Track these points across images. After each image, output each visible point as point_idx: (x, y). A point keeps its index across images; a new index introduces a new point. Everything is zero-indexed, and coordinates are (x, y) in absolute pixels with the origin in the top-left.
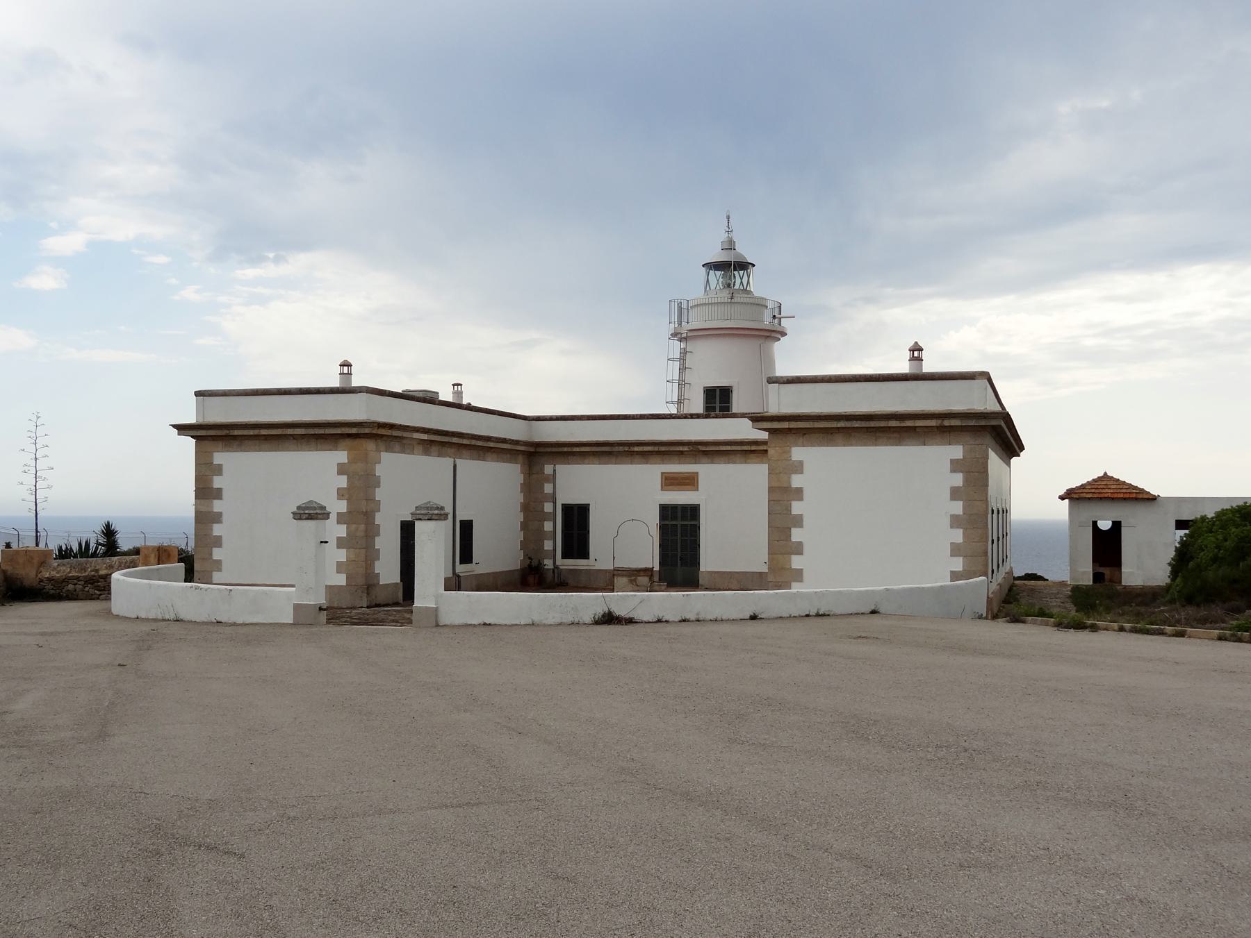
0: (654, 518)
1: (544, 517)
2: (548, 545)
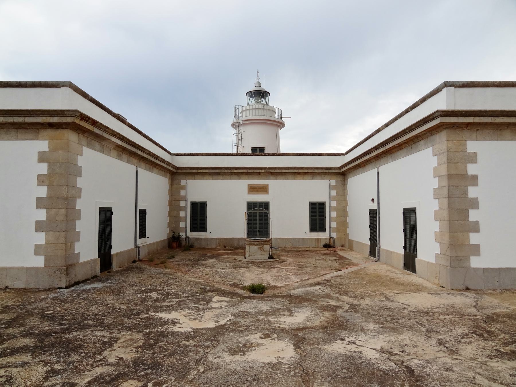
0: (243, 209)
1: (180, 209)
2: (182, 225)
